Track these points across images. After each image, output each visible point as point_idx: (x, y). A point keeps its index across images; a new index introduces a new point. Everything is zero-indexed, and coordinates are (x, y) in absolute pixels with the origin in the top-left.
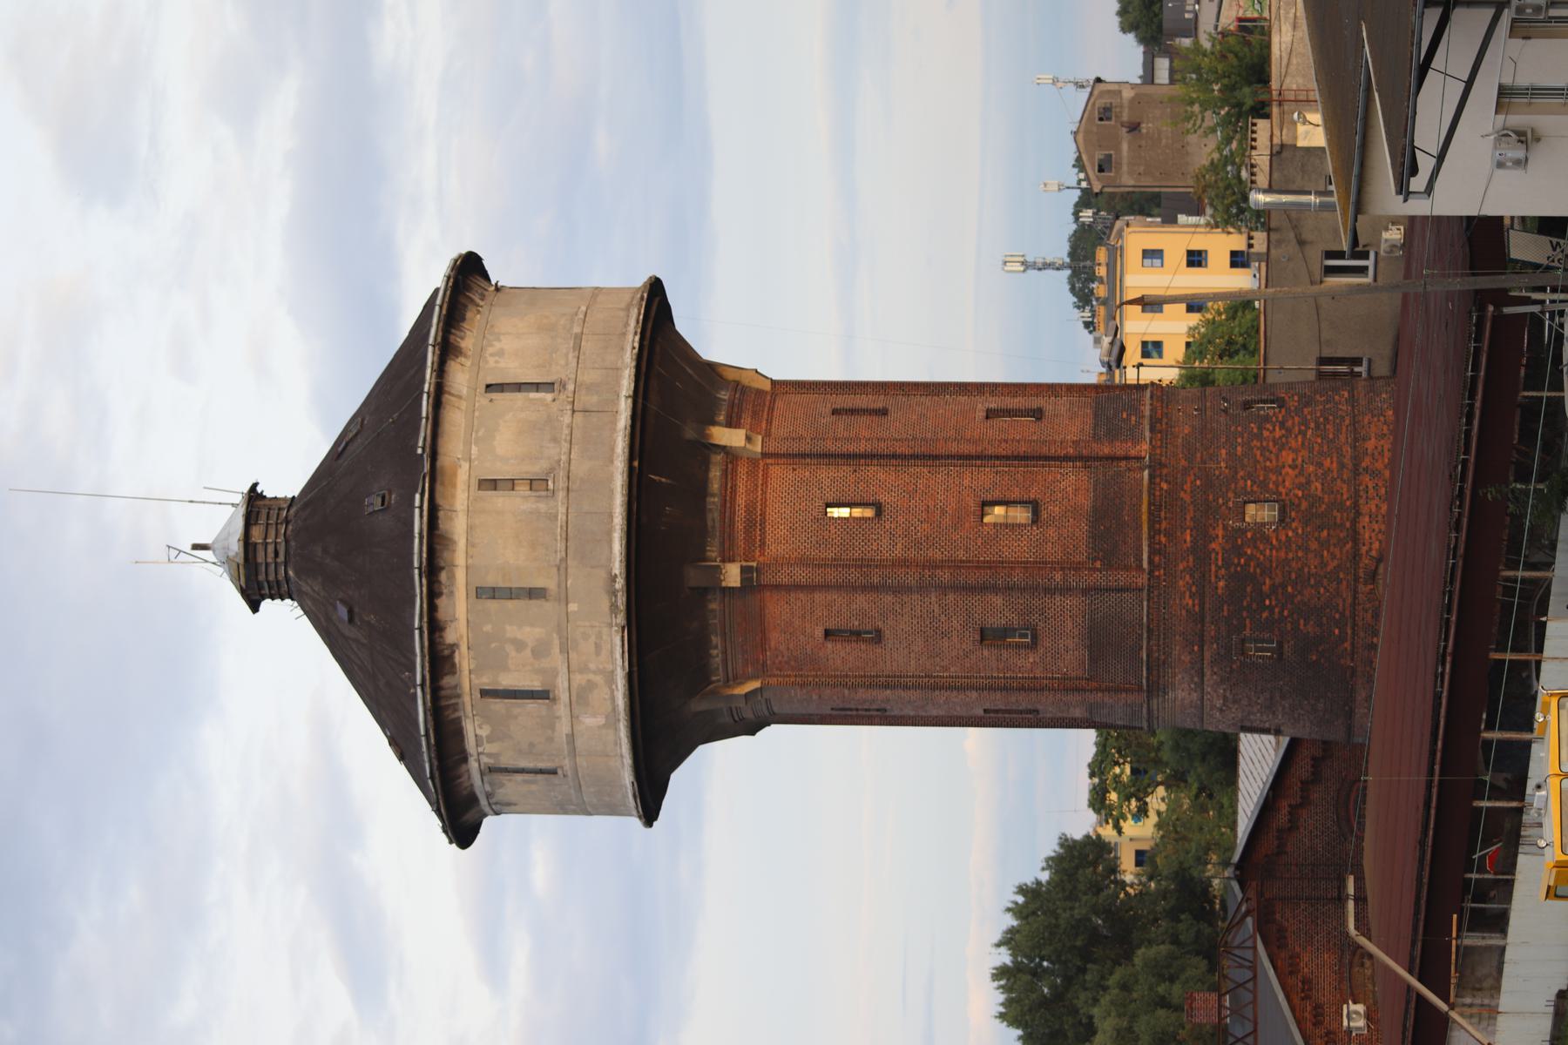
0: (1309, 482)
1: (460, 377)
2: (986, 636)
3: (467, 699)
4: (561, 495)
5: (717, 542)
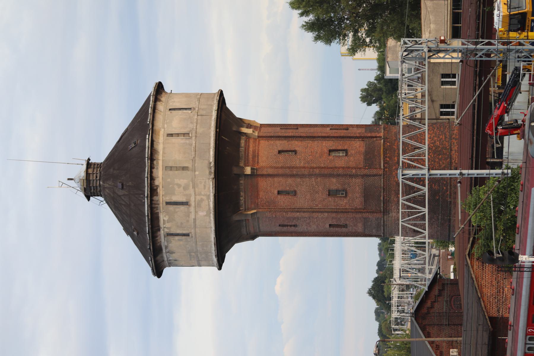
0: (435, 142)
1: (161, 106)
2: (330, 193)
3: (161, 205)
4: (194, 138)
5: (243, 161)
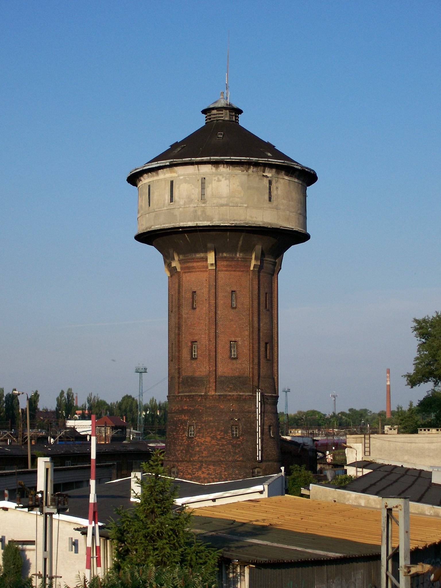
0: (199, 446)
